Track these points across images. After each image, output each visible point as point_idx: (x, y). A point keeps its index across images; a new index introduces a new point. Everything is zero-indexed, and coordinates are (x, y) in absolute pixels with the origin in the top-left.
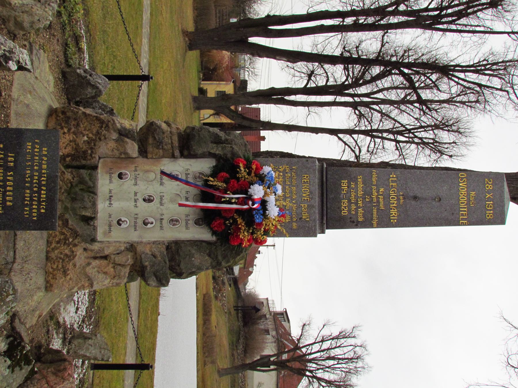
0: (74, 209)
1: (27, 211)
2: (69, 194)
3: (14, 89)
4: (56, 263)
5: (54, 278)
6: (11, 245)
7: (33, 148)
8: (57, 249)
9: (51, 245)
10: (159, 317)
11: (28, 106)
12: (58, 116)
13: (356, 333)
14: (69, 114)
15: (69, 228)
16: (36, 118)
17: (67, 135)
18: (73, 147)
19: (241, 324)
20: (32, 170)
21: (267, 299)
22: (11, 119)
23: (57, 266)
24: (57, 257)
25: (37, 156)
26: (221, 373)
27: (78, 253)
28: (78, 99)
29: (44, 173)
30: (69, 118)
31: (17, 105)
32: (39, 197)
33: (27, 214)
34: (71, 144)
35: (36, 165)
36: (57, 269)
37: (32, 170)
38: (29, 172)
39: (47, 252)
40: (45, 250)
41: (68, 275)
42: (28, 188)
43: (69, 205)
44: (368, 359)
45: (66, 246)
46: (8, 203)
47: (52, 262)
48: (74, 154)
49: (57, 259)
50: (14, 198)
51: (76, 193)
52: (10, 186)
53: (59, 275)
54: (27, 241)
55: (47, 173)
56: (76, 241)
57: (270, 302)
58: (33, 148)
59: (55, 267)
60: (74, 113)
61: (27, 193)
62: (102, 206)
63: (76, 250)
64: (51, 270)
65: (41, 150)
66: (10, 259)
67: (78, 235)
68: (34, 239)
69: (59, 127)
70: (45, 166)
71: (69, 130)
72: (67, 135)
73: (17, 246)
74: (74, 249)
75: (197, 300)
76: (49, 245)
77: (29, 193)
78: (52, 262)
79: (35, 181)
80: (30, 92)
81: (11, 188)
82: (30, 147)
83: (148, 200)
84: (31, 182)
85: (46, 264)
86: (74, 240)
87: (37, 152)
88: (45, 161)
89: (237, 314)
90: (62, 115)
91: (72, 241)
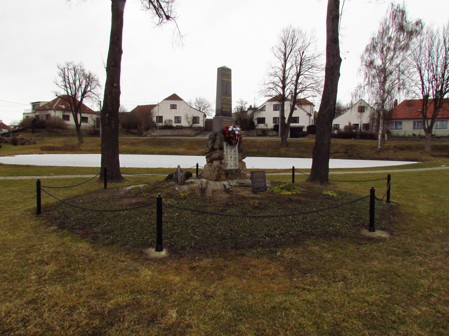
10: (126, 167)
13: (61, 67)
19: (43, 130)
21: (24, 114)
26: (81, 141)
44: (76, 63)
57: (26, 112)
62: (232, 168)
75: (48, 154)
83: (231, 157)
89: (37, 132)
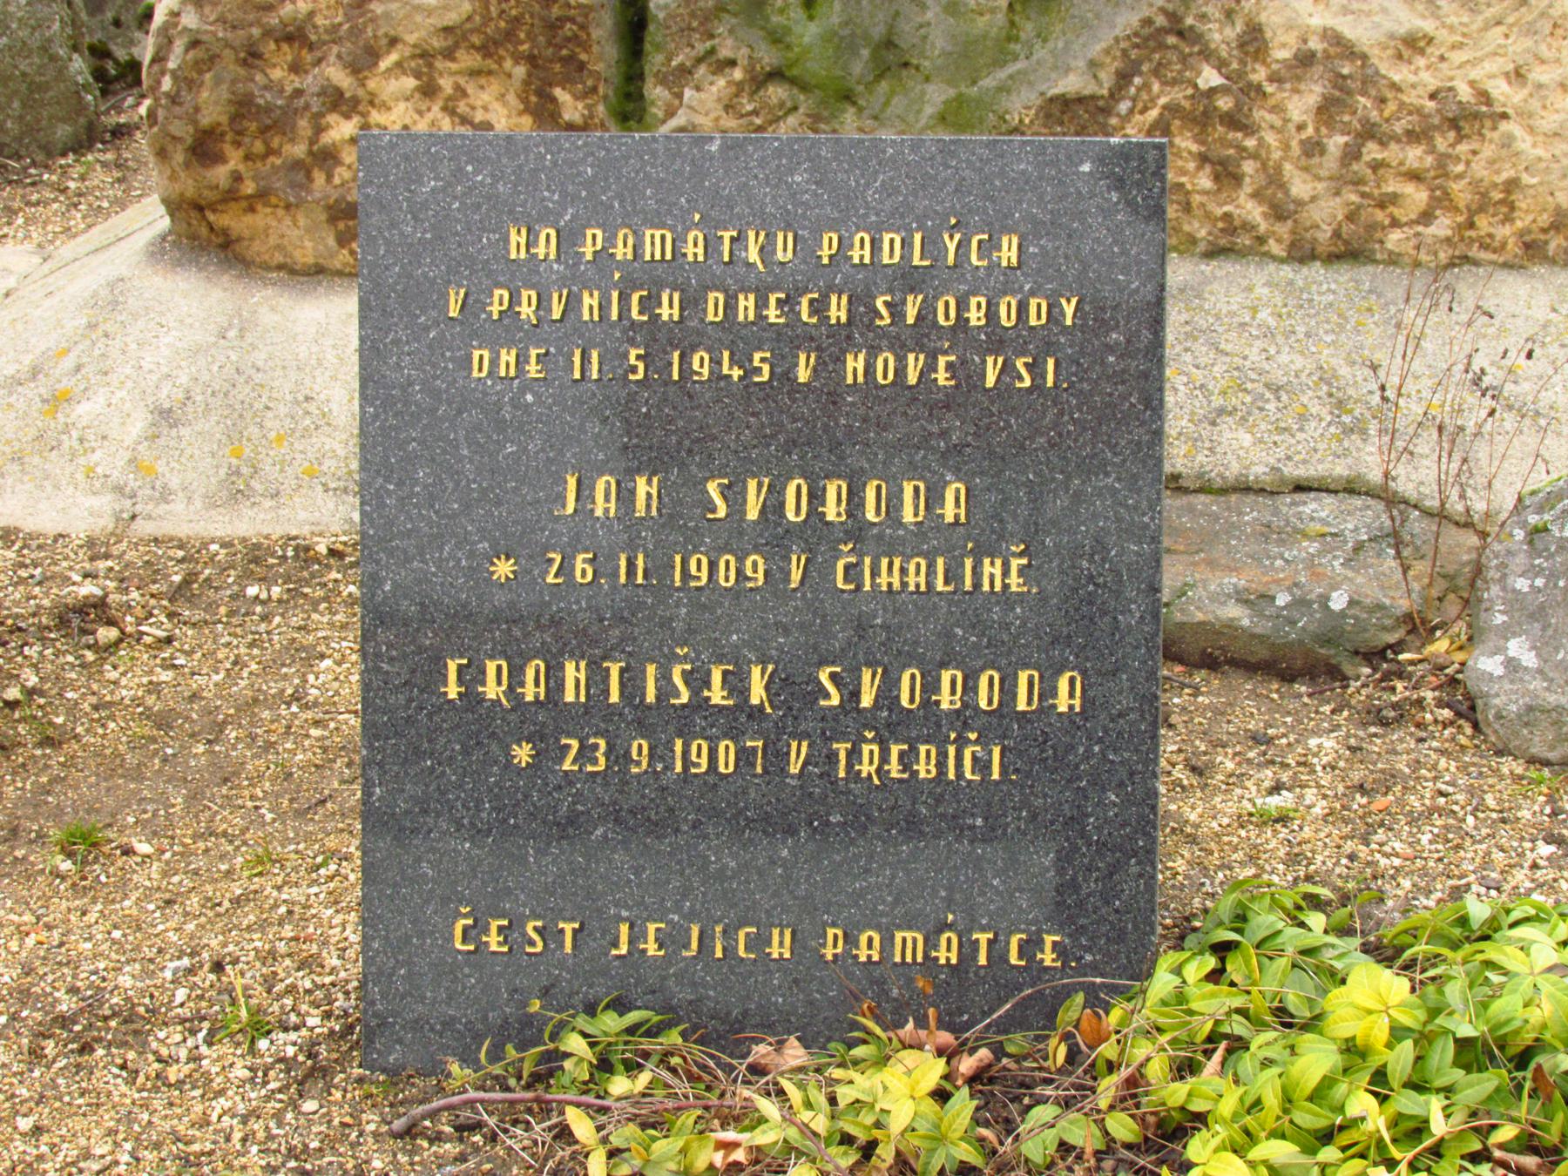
0: (969, 58)
1: (1007, 369)
2: (848, 97)
3: (42, 518)
4: (1391, 187)
5: (1506, 199)
6: (1252, 512)
7: (508, 329)
8: (1275, 179)
9: (1248, 227)
11: (166, 417)
12: (230, 196)
14: (212, 105)
15: (1115, 95)
16: (260, 357)
17: (376, 117)
18: (474, 73)
20: (686, 336)
22: (277, 532)
23: (1415, 176)
24: (1339, 183)
25: (572, 304)
27: (1316, 21)
28: (79, 66)
29: (711, 245)
30: (243, 107)
31: (165, 496)
32: (907, 279)
33: (1035, 368)
34: (446, 84)
35: (649, 303)
36: (1436, 178)
37: (686, 336)
38: (701, 363)
39: (1302, 253)
40: (1286, 271)
41: (1485, 97)
42: (830, 363)
43: (937, 95)
45: (1260, 115)
46: (949, 512)
47: (1380, 216)
48: (532, 60)
49: (1358, 182)
50: (913, 471)
51: (842, 43)
52: (817, 497)
53: (1479, 162)
54: (1217, 401)
55: (710, 225)
56: (1221, 36)
58: (508, 329)
59: (1417, 196)
60: (201, 66)
61: (869, 369)
63: (1291, 39)
64: (1442, 226)
65: (529, 273)
66: (1360, 519)
67: (1174, 17)
68: (1200, 348)
69: (319, 178)
70: (656, 242)
71: (338, 102)
72: (376, 117)
73: (1258, 471)
74: (1283, 54)
76: (1244, 240)
77: (873, 352)
78: (1380, 216)
79: (772, 314)
80: (57, 401)
81: (833, 490)
82: (508, 357)
84: (787, 340)
85: (1393, 260)
86: (1207, 54)
87: (543, 303)
88: (610, 240)
90: (220, 159)
91: (1221, 65)
